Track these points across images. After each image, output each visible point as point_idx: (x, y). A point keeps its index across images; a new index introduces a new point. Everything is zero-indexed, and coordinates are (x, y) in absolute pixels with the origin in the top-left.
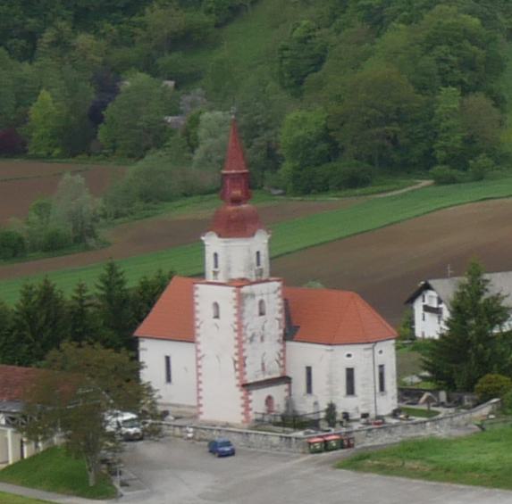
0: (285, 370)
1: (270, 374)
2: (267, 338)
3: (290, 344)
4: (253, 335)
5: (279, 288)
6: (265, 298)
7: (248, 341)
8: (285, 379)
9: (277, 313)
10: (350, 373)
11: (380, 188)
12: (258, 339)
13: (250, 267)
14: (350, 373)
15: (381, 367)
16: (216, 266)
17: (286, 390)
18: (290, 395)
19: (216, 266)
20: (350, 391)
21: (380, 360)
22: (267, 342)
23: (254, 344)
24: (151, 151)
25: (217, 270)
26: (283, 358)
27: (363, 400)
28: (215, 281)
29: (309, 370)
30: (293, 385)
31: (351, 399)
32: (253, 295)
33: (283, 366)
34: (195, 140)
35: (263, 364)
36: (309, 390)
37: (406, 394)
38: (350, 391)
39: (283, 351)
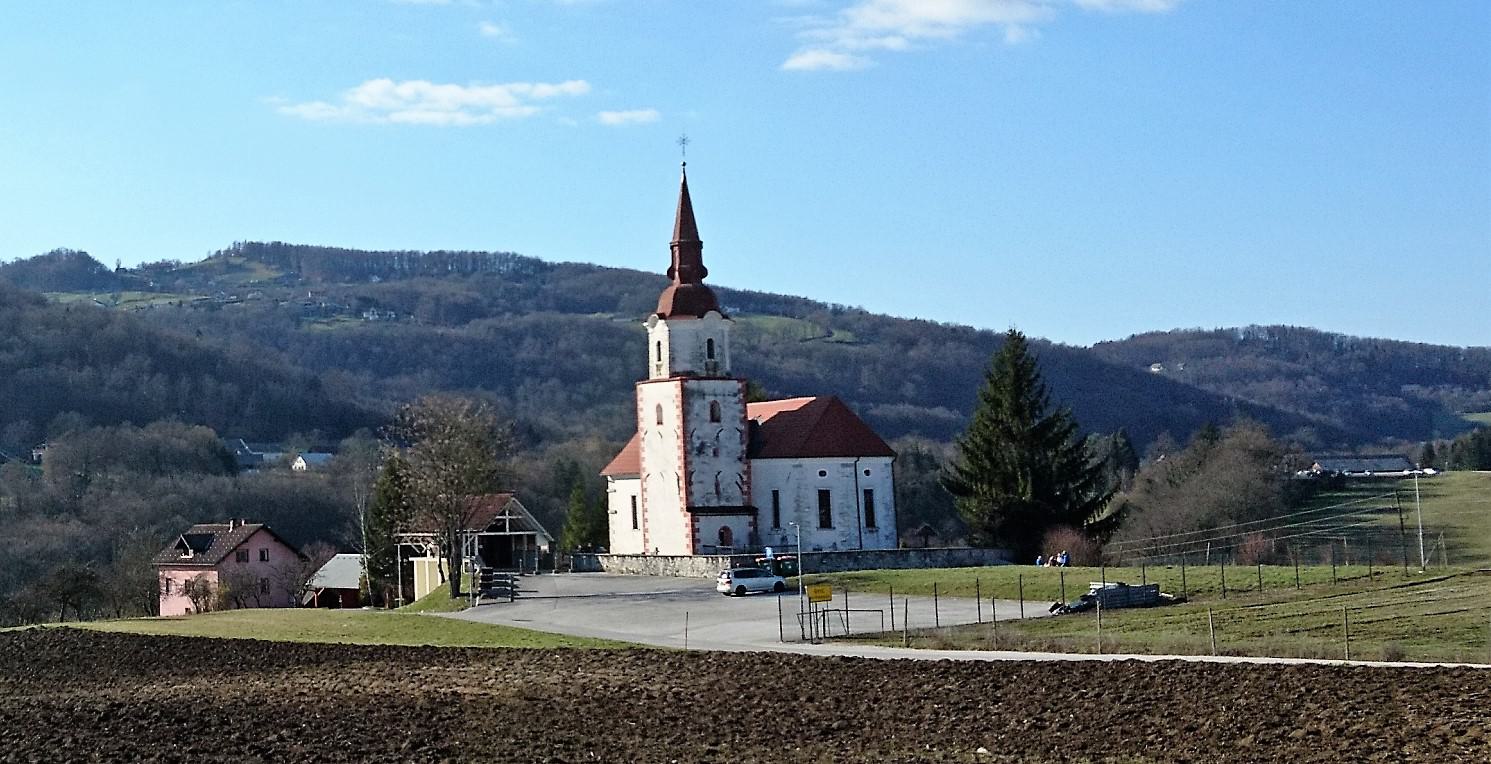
0: (749, 499)
1: (727, 500)
2: (723, 452)
3: (756, 463)
4: (703, 445)
5: (739, 391)
6: (719, 399)
7: (695, 452)
8: (749, 510)
9: (738, 422)
10: (824, 497)
11: (169, 295)
12: (710, 452)
13: (699, 357)
14: (824, 497)
15: (869, 493)
16: (659, 360)
17: (750, 524)
18: (756, 529)
19: (659, 360)
20: (826, 523)
21: (865, 482)
22: (723, 457)
23: (702, 458)
24: (62, 517)
25: (660, 363)
26: (746, 482)
27: (842, 534)
28: (660, 377)
29: (776, 494)
30: (759, 517)
31: (825, 532)
32: (702, 395)
33: (748, 493)
34: (507, 260)
35: (717, 485)
36: (777, 524)
37: (712, 406)
38: (826, 523)
39: (748, 472)
